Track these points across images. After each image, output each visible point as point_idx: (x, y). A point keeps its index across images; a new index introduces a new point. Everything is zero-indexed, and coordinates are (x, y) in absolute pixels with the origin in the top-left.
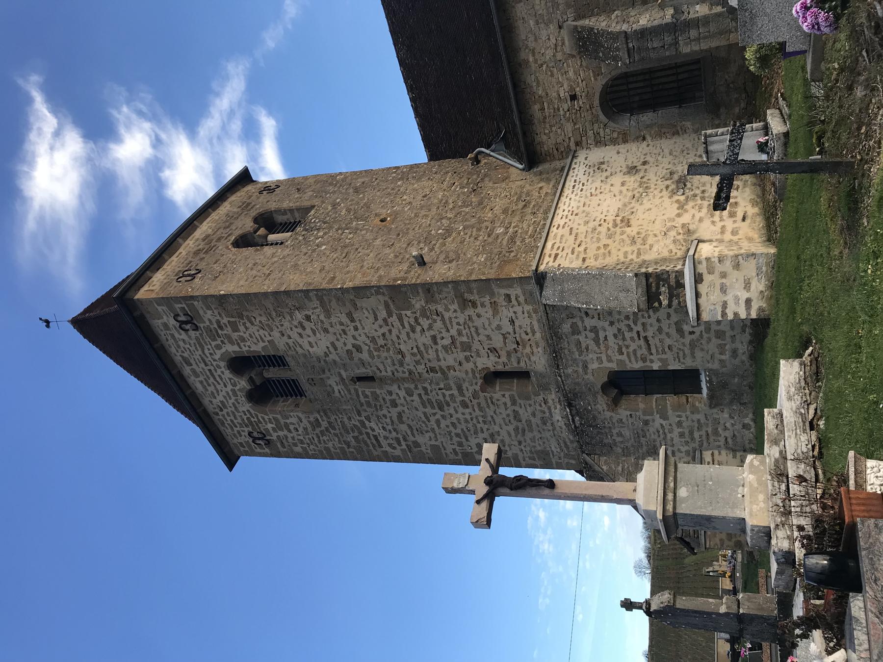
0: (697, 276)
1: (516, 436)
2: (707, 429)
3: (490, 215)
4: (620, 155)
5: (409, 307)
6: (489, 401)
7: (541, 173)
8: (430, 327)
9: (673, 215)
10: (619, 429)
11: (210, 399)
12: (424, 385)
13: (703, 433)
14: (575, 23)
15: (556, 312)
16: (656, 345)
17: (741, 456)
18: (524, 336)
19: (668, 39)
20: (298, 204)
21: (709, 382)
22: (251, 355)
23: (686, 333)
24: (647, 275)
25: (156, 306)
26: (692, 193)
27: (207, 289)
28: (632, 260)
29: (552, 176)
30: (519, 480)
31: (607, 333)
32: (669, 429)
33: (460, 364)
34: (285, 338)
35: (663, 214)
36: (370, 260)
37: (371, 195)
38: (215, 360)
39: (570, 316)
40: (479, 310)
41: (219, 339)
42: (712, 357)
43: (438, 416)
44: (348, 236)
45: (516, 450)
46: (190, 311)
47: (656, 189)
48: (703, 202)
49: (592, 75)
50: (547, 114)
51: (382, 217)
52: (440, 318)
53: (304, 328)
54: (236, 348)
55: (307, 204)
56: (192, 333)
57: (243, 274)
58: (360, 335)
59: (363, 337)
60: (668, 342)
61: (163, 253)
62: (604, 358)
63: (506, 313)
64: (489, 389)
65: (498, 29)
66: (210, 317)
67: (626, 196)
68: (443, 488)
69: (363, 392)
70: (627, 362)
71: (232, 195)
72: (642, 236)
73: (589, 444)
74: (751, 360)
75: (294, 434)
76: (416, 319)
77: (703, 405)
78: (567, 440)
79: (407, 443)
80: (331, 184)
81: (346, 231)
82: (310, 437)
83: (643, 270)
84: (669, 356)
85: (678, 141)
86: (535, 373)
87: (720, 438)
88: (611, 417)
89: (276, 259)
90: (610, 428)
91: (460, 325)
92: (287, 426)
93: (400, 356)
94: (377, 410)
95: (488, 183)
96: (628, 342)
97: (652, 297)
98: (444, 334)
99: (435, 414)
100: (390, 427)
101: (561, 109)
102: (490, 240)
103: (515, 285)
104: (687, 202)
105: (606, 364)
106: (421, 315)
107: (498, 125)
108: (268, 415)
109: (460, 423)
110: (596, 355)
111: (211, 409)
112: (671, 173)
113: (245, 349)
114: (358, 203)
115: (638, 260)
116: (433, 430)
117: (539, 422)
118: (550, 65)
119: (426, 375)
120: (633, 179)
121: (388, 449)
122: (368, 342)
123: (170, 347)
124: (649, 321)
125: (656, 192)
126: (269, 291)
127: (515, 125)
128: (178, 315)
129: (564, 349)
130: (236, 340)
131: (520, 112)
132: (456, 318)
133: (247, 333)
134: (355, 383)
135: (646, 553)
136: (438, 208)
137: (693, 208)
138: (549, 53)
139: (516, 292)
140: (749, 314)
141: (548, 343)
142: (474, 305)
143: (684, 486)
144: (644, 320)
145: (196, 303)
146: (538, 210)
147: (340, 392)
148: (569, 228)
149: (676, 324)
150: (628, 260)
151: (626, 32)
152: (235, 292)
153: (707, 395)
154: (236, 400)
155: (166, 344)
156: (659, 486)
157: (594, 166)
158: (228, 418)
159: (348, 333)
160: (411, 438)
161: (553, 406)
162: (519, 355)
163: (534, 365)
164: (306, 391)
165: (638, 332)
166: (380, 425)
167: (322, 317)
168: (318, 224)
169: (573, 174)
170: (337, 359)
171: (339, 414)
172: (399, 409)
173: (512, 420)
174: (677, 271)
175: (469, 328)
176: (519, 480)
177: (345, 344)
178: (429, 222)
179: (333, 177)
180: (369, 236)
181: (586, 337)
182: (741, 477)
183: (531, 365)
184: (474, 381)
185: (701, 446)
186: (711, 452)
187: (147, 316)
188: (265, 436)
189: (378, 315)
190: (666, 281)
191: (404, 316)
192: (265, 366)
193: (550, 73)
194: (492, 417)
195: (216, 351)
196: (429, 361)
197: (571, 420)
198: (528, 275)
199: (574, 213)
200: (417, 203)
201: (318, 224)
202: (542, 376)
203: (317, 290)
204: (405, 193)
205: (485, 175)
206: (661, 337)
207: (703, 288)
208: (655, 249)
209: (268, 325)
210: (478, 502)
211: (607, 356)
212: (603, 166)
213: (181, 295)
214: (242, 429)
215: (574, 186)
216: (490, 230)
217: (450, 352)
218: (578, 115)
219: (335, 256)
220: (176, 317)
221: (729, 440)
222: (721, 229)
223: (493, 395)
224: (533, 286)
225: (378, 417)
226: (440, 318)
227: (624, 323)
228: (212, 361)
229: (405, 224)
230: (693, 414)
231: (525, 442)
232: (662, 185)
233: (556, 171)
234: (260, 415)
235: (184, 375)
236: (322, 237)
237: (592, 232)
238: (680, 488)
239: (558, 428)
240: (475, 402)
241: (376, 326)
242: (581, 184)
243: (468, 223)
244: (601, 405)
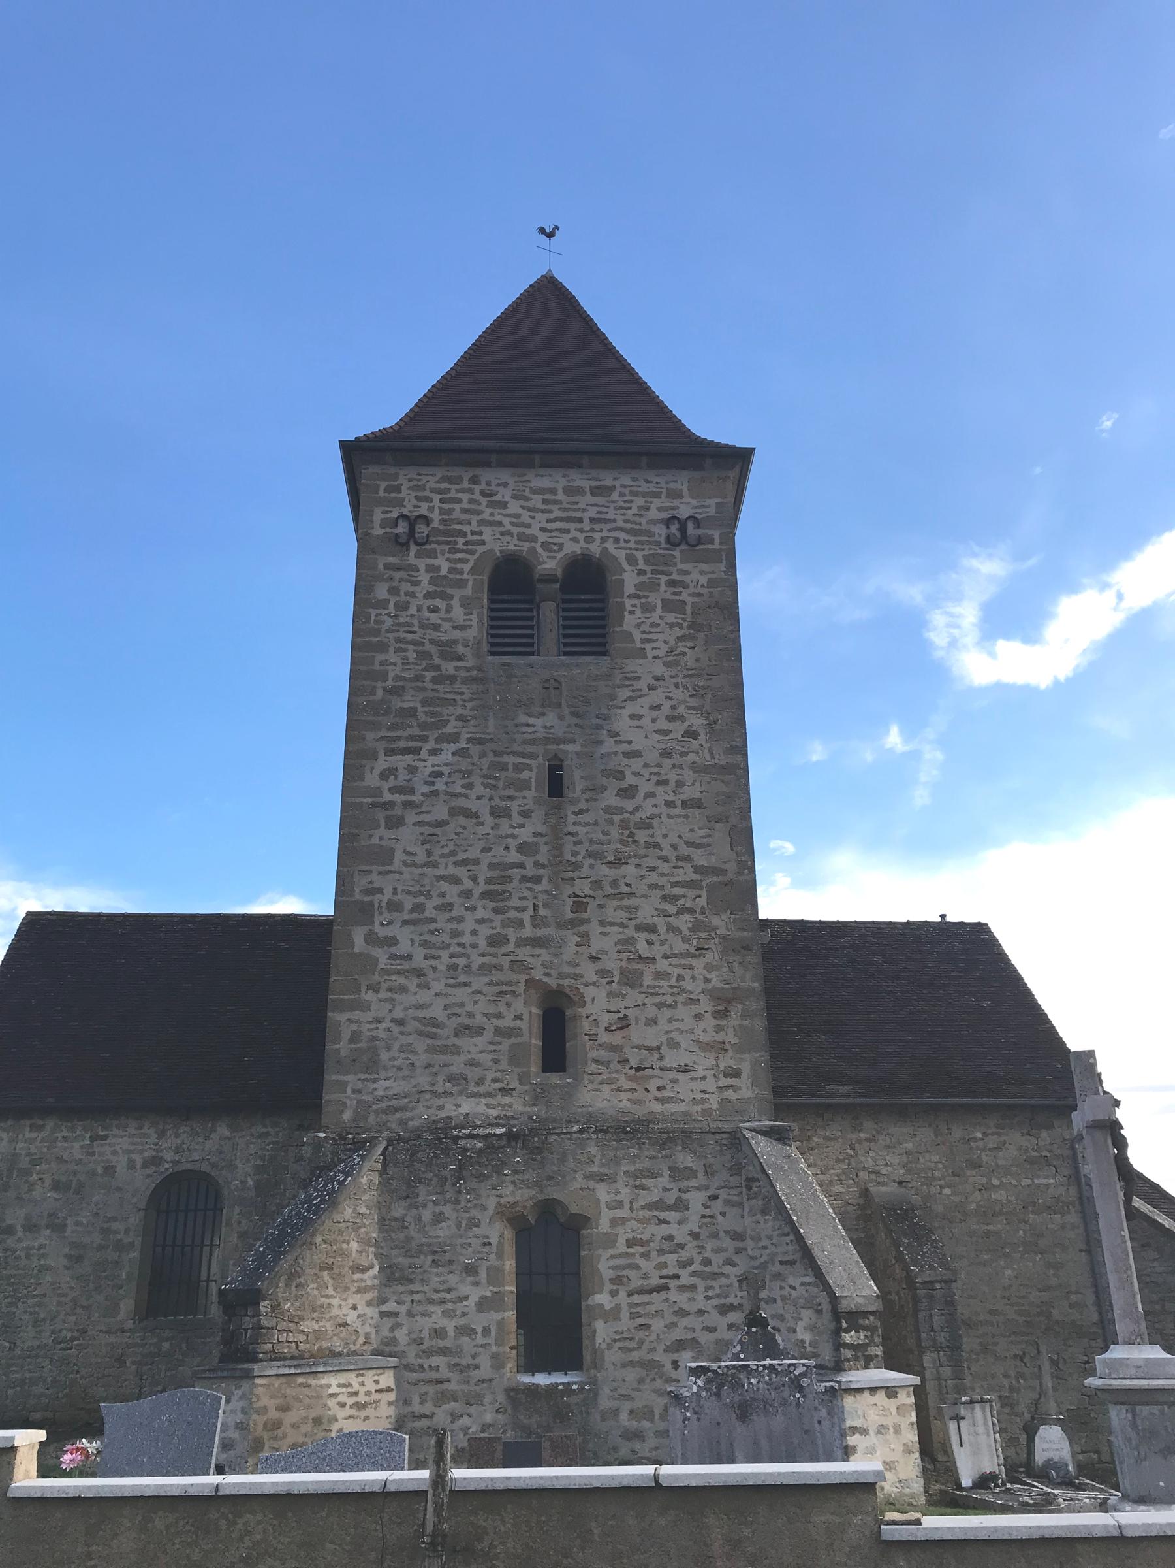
1: (419, 1020)
2: (453, 1382)
8: (671, 929)
12: (545, 881)
13: (444, 1373)
18: (657, 1082)
19: (942, 1338)
23: (675, 1356)
32: (454, 1311)
38: (603, 540)
40: (710, 1022)
43: (468, 884)
54: (629, 589)
60: (657, 1325)
62: (619, 1213)
63: (703, 1063)
70: (611, 1252)
73: (412, 1156)
76: (691, 911)
78: (408, 1114)
90: (458, 1202)
93: (611, 859)
96: (656, 1259)
99: (474, 879)
105: (606, 1216)
106: (698, 921)
108: (473, 571)
117: (455, 1070)
124: (700, 1297)
129: (640, 1148)
138: (869, 1163)
139: (744, 1090)
144: (701, 1289)
159: (661, 788)
160: (411, 817)
162: (614, 1066)
163: (590, 1087)
165: (677, 1277)
167: (692, 757)
177: (637, 774)
181: (665, 1190)
184: (554, 973)
185: (408, 1367)
186: (393, 1387)
187: (696, 474)
188: (417, 544)
239: (439, 1102)
244: (513, 1193)
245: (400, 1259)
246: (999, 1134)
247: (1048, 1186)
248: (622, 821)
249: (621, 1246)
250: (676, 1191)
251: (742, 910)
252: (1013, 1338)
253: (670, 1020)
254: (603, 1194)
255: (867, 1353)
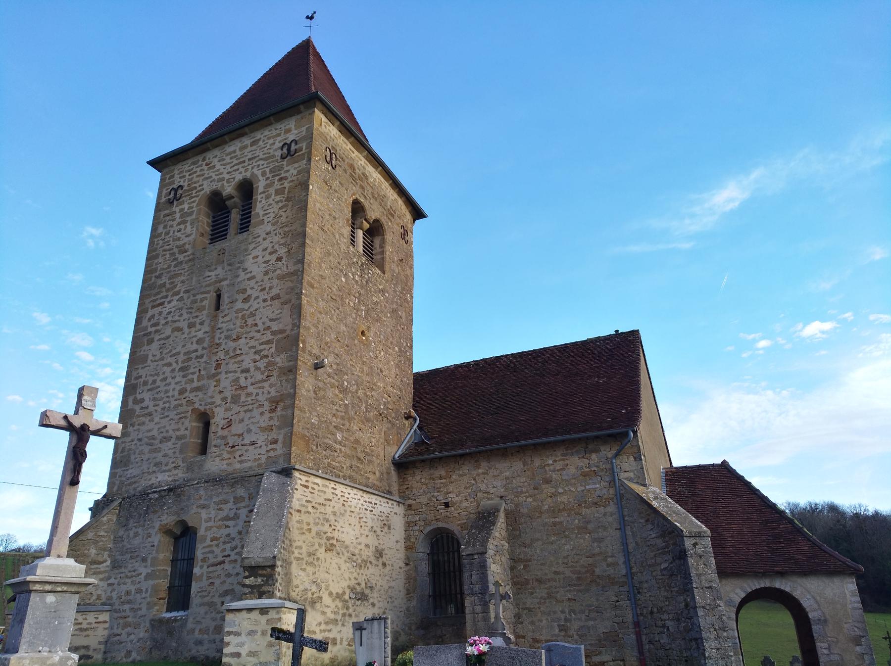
0: (266, 610)
1: (147, 437)
3: (355, 428)
4: (395, 543)
5: (278, 351)
6: (183, 415)
7: (388, 473)
8: (257, 368)
9: (331, 589)
10: (141, 534)
11: (218, 157)
12: (205, 357)
13: (128, 613)
14: (502, 510)
15: (256, 484)
16: (216, 571)
17: (100, 649)
19: (477, 588)
20: (388, 259)
21: (176, 620)
22: (253, 201)
23: (222, 599)
24: (273, 567)
25: (307, 126)
26: (350, 606)
27: (316, 174)
28: (293, 553)
29: (385, 484)
30: (82, 455)
31: (232, 528)
33: (221, 392)
34: (265, 236)
35: (333, 581)
36: (326, 320)
37: (388, 324)
38: (253, 168)
39: (251, 496)
41: (270, 176)
42: (199, 622)
43: (174, 365)
44: (351, 302)
45: (133, 435)
46: (299, 155)
47: (359, 574)
48: (341, 615)
49: (463, 522)
50: (436, 482)
51: (366, 332)
52: (264, 378)
53: (271, 253)
54: (261, 189)
55: (387, 267)
56: (279, 153)
57: (326, 207)
58: (258, 303)
59: (257, 306)
60: (217, 582)
61: (355, 137)
62: (209, 524)
63: (261, 439)
64: (194, 416)
65: (505, 445)
66: (291, 172)
67: (355, 548)
68: (84, 386)
69: (206, 298)
71: (403, 202)
72: (315, 562)
74: (191, 658)
75: (176, 228)
76: (266, 356)
77: (154, 613)
79: (153, 333)
80: (403, 289)
81: (357, 300)
82: (170, 243)
83: (279, 563)
84: (205, 583)
85: (402, 593)
86: (204, 460)
87: (120, 629)
88: (154, 527)
89: (337, 237)
90: (144, 526)
91: (256, 396)
92: (184, 222)
93: (234, 337)
94: (188, 309)
95: (385, 426)
96: (222, 547)
97: (253, 570)
98: (250, 381)
99: (177, 362)
100: (170, 318)
101: (439, 494)
102: (331, 428)
103: (284, 449)
104: (343, 601)
105: (204, 525)
107: (434, 438)
108: (197, 205)
109: (165, 385)
110: (213, 517)
111: (209, 155)
112: (371, 588)
113: (259, 197)
114: (382, 312)
115: (293, 558)
116: (162, 359)
117: (158, 460)
118: (474, 487)
119: (214, 358)
120: (370, 554)
121: (149, 314)
122: (252, 309)
123: (270, 131)
125: (355, 575)
126: (307, 229)
127: (430, 454)
128: (296, 144)
129: (222, 489)
130: (268, 191)
131: (440, 458)
132: (263, 393)
133: (273, 202)
134: (215, 292)
135: (24, 547)
136: (368, 382)
137: (336, 606)
138: (483, 487)
140: (227, 655)
141: (230, 474)
142: (272, 411)
143: (57, 599)
145: (304, 162)
146: (354, 470)
147: (209, 276)
148: (332, 498)
149: (233, 590)
150: (294, 549)
151: (486, 553)
152: (310, 199)
153: (164, 617)
154: (214, 180)
155: (272, 127)
156: (59, 578)
157: (388, 521)
158: (198, 169)
159: (262, 293)
160: (157, 337)
161: (171, 474)
162: (223, 447)
163: (211, 460)
164: (214, 246)
165: (229, 556)
166: (173, 310)
167: (278, 272)
168: (366, 276)
169: (382, 502)
170: (239, 279)
171: (189, 272)
172: (186, 330)
173: (162, 435)
174: (273, 592)
175: (252, 404)
176: (82, 455)
177: (252, 288)
178: (356, 373)
179: (410, 290)
180: (350, 320)
181: (231, 509)
182: (58, 649)
183: (211, 457)
184: (203, 403)
185: (115, 611)
187: (299, 117)
189: (275, 323)
190: (266, 583)
191: (270, 346)
192: (243, 211)
193: (468, 486)
194: (167, 416)
195: (261, 171)
196: (227, 364)
197: (155, 490)
198: (292, 461)
199: (345, 503)
200: (376, 364)
201: (366, 276)
202: (201, 466)
203: (303, 271)
204: (386, 353)
205: (393, 425)
206: (222, 576)
207: (255, 615)
208: (301, 573)
209: (277, 222)
210: (66, 417)
211: (211, 527)
212: (386, 528)
213: (313, 150)
214: (187, 180)
215: (371, 503)
216: (341, 428)
217: (233, 384)
218: (432, 508)
219: (334, 290)
220: (296, 142)
221: (117, 638)
222: (313, 631)
223: (188, 420)
224: (282, 465)
225: (181, 309)
226: (264, 378)
227: (239, 543)
228: (252, 165)
229: (357, 353)
230: (147, 604)
231: (140, 445)
232: (362, 579)
233: (389, 487)
234: (197, 199)
235: (243, 138)
236: (354, 279)
237: (325, 518)
238: (55, 597)
239: (149, 477)
240: (184, 402)
241: (265, 319)
242: (372, 509)
243: (350, 408)
244: (166, 519)
245: (119, 557)
246: (563, 460)
247: (595, 490)
248: (242, 316)
249: (208, 542)
250: (235, 510)
251: (291, 350)
252: (568, 588)
253: (250, 418)
254: (204, 515)
255: (261, 590)
